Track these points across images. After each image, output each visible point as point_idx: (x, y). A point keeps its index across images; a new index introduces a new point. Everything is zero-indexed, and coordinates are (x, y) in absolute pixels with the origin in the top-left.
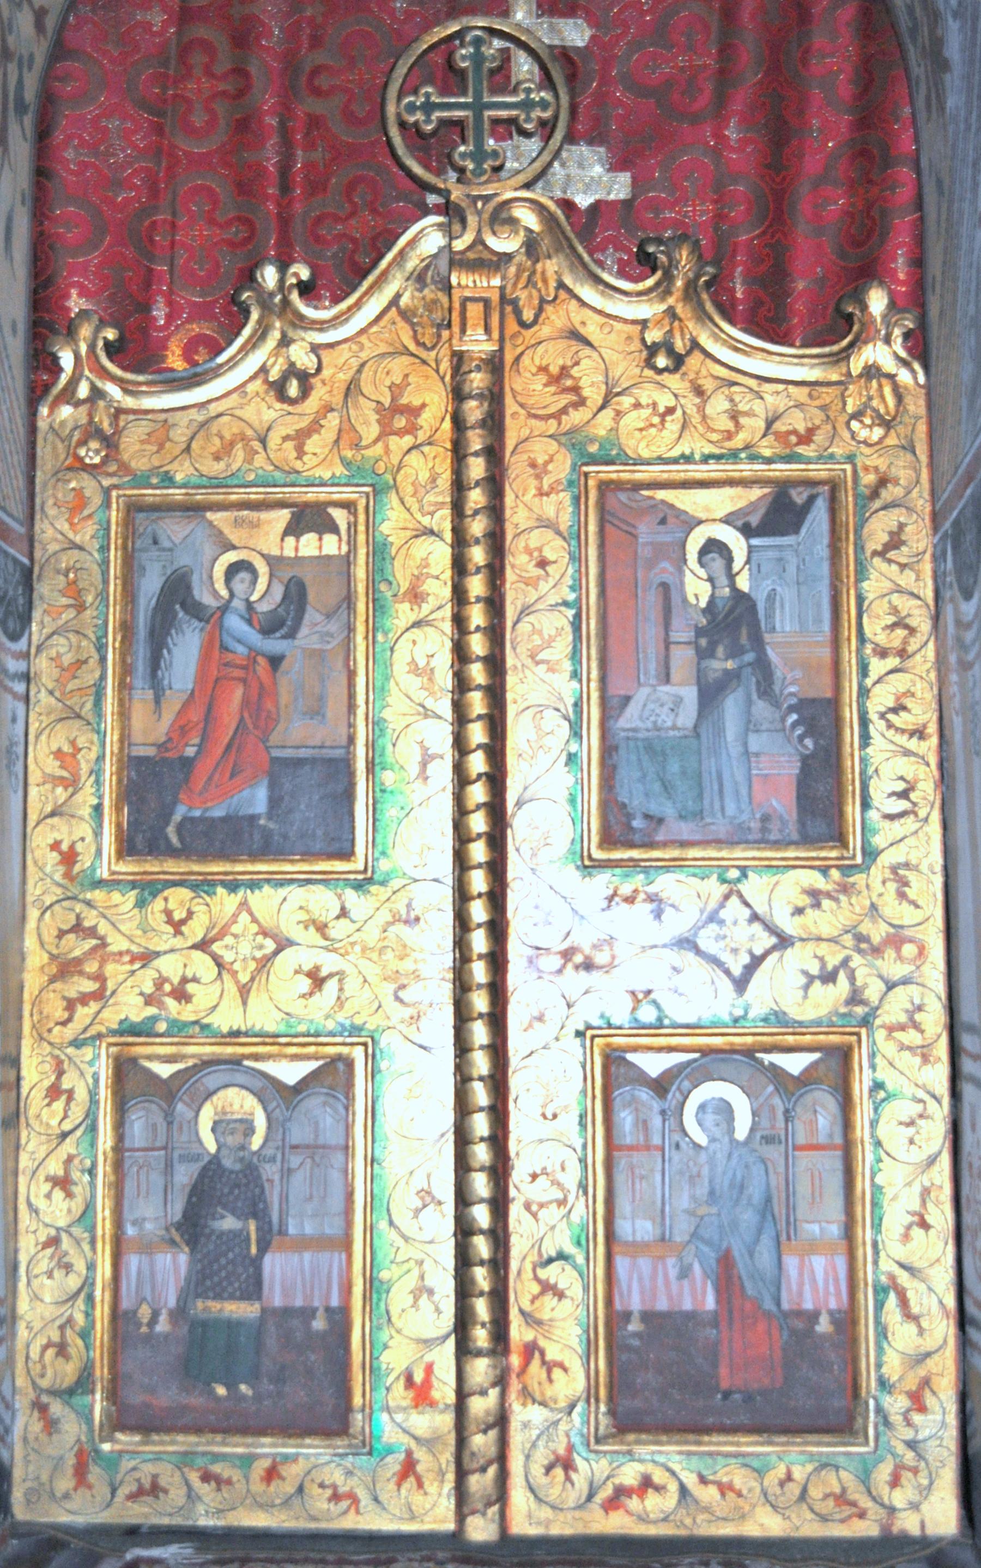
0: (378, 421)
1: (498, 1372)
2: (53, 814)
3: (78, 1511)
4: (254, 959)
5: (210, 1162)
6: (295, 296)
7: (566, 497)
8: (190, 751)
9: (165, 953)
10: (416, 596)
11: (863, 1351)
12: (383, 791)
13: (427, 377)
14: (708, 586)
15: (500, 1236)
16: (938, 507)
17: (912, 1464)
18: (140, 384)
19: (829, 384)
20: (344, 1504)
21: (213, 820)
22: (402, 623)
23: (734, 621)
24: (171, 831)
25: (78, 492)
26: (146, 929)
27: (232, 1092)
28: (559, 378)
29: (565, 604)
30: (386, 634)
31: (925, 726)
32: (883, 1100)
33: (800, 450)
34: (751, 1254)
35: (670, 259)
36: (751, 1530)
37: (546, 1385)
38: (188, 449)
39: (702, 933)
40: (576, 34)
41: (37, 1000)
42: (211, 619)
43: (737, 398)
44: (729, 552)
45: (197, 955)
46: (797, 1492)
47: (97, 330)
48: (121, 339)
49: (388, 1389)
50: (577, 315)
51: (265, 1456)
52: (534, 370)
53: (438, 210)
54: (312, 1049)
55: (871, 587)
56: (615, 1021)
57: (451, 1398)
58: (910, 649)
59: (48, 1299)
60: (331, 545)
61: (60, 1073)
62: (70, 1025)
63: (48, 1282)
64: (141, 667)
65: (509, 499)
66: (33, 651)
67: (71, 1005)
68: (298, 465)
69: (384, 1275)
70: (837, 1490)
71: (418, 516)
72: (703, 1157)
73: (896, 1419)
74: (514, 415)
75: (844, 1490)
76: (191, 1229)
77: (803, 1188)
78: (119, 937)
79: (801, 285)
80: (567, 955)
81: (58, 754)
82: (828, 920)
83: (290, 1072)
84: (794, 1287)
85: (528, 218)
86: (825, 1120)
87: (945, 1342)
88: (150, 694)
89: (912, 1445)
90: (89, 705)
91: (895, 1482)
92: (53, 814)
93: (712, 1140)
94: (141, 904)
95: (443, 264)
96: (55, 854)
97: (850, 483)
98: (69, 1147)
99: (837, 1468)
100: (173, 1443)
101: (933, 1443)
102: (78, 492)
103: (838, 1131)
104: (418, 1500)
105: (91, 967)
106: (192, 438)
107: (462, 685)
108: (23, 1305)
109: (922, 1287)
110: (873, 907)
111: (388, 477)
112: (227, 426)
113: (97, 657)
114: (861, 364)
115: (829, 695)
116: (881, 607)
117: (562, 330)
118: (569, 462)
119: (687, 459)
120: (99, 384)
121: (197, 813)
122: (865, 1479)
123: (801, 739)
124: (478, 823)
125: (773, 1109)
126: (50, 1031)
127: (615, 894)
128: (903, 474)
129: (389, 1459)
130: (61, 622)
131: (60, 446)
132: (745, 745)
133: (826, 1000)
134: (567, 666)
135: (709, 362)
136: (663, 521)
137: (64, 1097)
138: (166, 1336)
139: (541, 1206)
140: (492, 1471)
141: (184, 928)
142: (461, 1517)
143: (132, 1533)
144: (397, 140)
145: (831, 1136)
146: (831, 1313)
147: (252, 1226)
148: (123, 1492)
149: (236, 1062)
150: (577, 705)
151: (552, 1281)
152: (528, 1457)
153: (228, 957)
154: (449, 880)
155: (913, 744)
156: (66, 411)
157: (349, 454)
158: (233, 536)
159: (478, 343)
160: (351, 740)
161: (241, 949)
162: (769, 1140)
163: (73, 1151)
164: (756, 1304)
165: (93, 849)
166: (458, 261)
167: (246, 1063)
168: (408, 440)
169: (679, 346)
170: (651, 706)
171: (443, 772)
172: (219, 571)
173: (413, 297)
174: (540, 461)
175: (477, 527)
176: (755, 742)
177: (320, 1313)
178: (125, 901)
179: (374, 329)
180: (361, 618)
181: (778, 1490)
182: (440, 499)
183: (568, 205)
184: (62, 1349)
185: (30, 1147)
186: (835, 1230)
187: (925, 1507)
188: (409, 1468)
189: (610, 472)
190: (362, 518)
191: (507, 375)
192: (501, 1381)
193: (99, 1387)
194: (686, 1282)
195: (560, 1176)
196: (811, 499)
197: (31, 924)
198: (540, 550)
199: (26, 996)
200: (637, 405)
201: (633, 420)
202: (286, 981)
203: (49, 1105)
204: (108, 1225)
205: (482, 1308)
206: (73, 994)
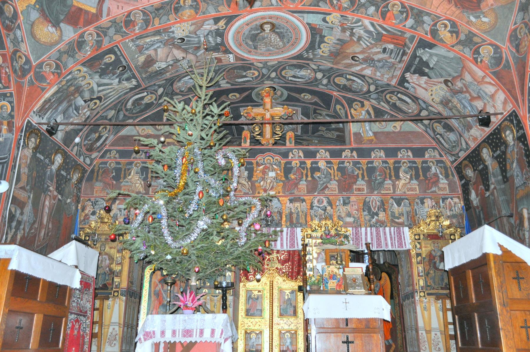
28: (277, 282)
83: (258, 332)
86: (295, 336)
161: (254, 323)
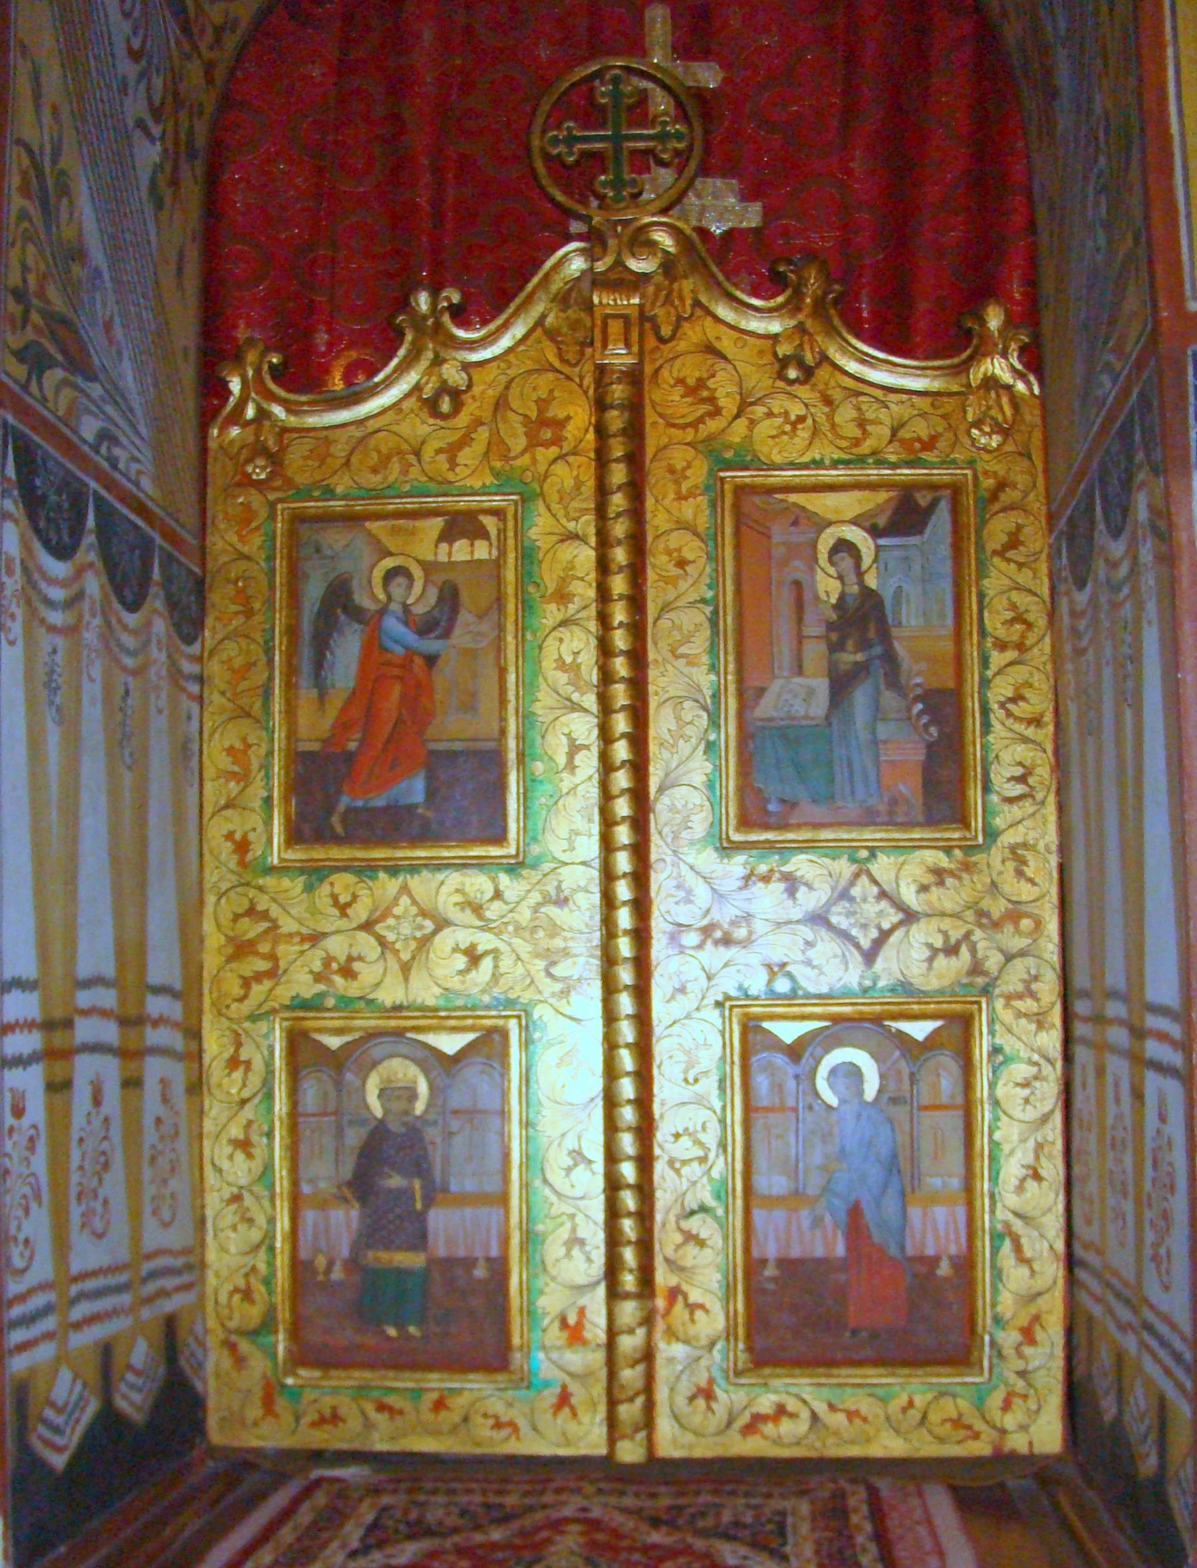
0: (526, 434)
1: (644, 1314)
2: (227, 806)
3: (269, 1436)
4: (415, 938)
5: (376, 1127)
6: (446, 319)
7: (703, 501)
8: (352, 746)
9: (333, 933)
10: (562, 597)
11: (979, 1293)
12: (533, 781)
13: (571, 392)
14: (837, 584)
15: (645, 1190)
16: (1053, 509)
17: (1023, 1392)
18: (303, 404)
19: (951, 394)
20: (504, 1432)
21: (374, 809)
22: (549, 622)
23: (863, 618)
24: (335, 820)
25: (247, 506)
26: (314, 911)
27: (396, 1063)
28: (696, 390)
29: (703, 601)
30: (534, 633)
31: (1042, 715)
32: (1001, 1064)
33: (924, 455)
34: (878, 1205)
35: (800, 277)
36: (875, 1450)
37: (689, 1325)
38: (347, 463)
39: (834, 909)
40: (708, 76)
41: (216, 979)
42: (371, 622)
43: (864, 407)
44: (858, 551)
45: (362, 936)
46: (919, 1416)
47: (263, 355)
48: (285, 363)
49: (544, 1331)
50: (711, 330)
51: (433, 1390)
52: (672, 382)
53: (580, 237)
54: (470, 1022)
55: (993, 584)
56: (753, 992)
57: (602, 1337)
58: (1028, 643)
59: (233, 1250)
60: (482, 551)
61: (239, 1045)
62: (246, 1002)
63: (233, 1235)
64: (306, 668)
65: (650, 503)
66: (206, 654)
67: (246, 983)
68: (451, 476)
69: (540, 1227)
70: (954, 1415)
71: (564, 521)
72: (834, 1117)
73: (1009, 1351)
74: (654, 423)
75: (960, 1415)
76: (361, 1185)
77: (926, 1146)
78: (290, 920)
79: (923, 306)
80: (707, 931)
81: (231, 751)
82: (949, 897)
83: (450, 1044)
84: (918, 1236)
85: (665, 240)
86: (947, 1084)
87: (1055, 1282)
88: (314, 692)
89: (1022, 1374)
90: (258, 704)
91: (1007, 1406)
92: (227, 806)
93: (843, 1101)
94: (309, 888)
95: (586, 284)
96: (229, 844)
97: (971, 487)
98: (248, 1112)
99: (954, 1396)
100: (350, 1378)
101: (1042, 1372)
102: (247, 506)
103: (959, 1089)
104: (572, 1427)
105: (264, 948)
106: (351, 453)
107: (607, 677)
108: (211, 1255)
109: (1035, 1234)
110: (994, 884)
111: (536, 486)
112: (384, 442)
113: (264, 659)
114: (980, 376)
115: (951, 684)
116: (1000, 604)
117: (696, 345)
118: (706, 468)
119: (817, 464)
120: (265, 406)
121: (360, 803)
122: (979, 1406)
123: (926, 726)
124: (622, 807)
125: (899, 1072)
126: (228, 1007)
127: (752, 874)
128: (1021, 480)
129: (546, 1393)
130: (231, 628)
131: (229, 463)
132: (874, 732)
133: (950, 968)
134: (705, 659)
135: (838, 374)
136: (795, 523)
137: (242, 1069)
138: (341, 1284)
139: (685, 1162)
140: (640, 1401)
141: (348, 911)
142: (612, 1441)
143: (317, 1456)
144: (541, 170)
145: (952, 1097)
146: (951, 1258)
147: (417, 1184)
148: (305, 1421)
149: (399, 1033)
150: (716, 696)
151: (694, 1232)
152: (672, 1389)
153: (391, 937)
154: (596, 863)
155: (1030, 732)
156: (235, 431)
157: (498, 464)
158: (390, 543)
159: (619, 356)
160: (503, 732)
162: (894, 1101)
163: (251, 1116)
164: (881, 1250)
165: (264, 839)
166: (598, 282)
167: (409, 1035)
168: (553, 451)
169: (809, 359)
170: (786, 696)
171: (588, 763)
172: (378, 574)
173: (557, 317)
174: (679, 467)
175: (620, 529)
176: (883, 731)
177: (482, 1262)
178: (294, 886)
179: (522, 348)
180: (511, 619)
181: (900, 1416)
182: (585, 505)
183: (703, 233)
184: (247, 1294)
185: (214, 1113)
186: (956, 1183)
187: (1032, 1429)
188: (564, 1399)
189: (744, 476)
190: (510, 524)
191: (646, 388)
192: (648, 1321)
193: (281, 1328)
194: (818, 1233)
195: (702, 1137)
196: (934, 504)
197: (209, 909)
198: (679, 550)
199: (205, 974)
200: (770, 414)
201: (765, 428)
202: (445, 960)
203: (229, 1075)
204: (286, 1183)
205: (629, 1255)
206: (248, 973)
